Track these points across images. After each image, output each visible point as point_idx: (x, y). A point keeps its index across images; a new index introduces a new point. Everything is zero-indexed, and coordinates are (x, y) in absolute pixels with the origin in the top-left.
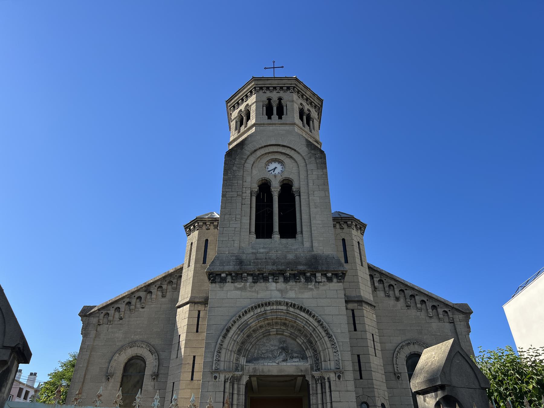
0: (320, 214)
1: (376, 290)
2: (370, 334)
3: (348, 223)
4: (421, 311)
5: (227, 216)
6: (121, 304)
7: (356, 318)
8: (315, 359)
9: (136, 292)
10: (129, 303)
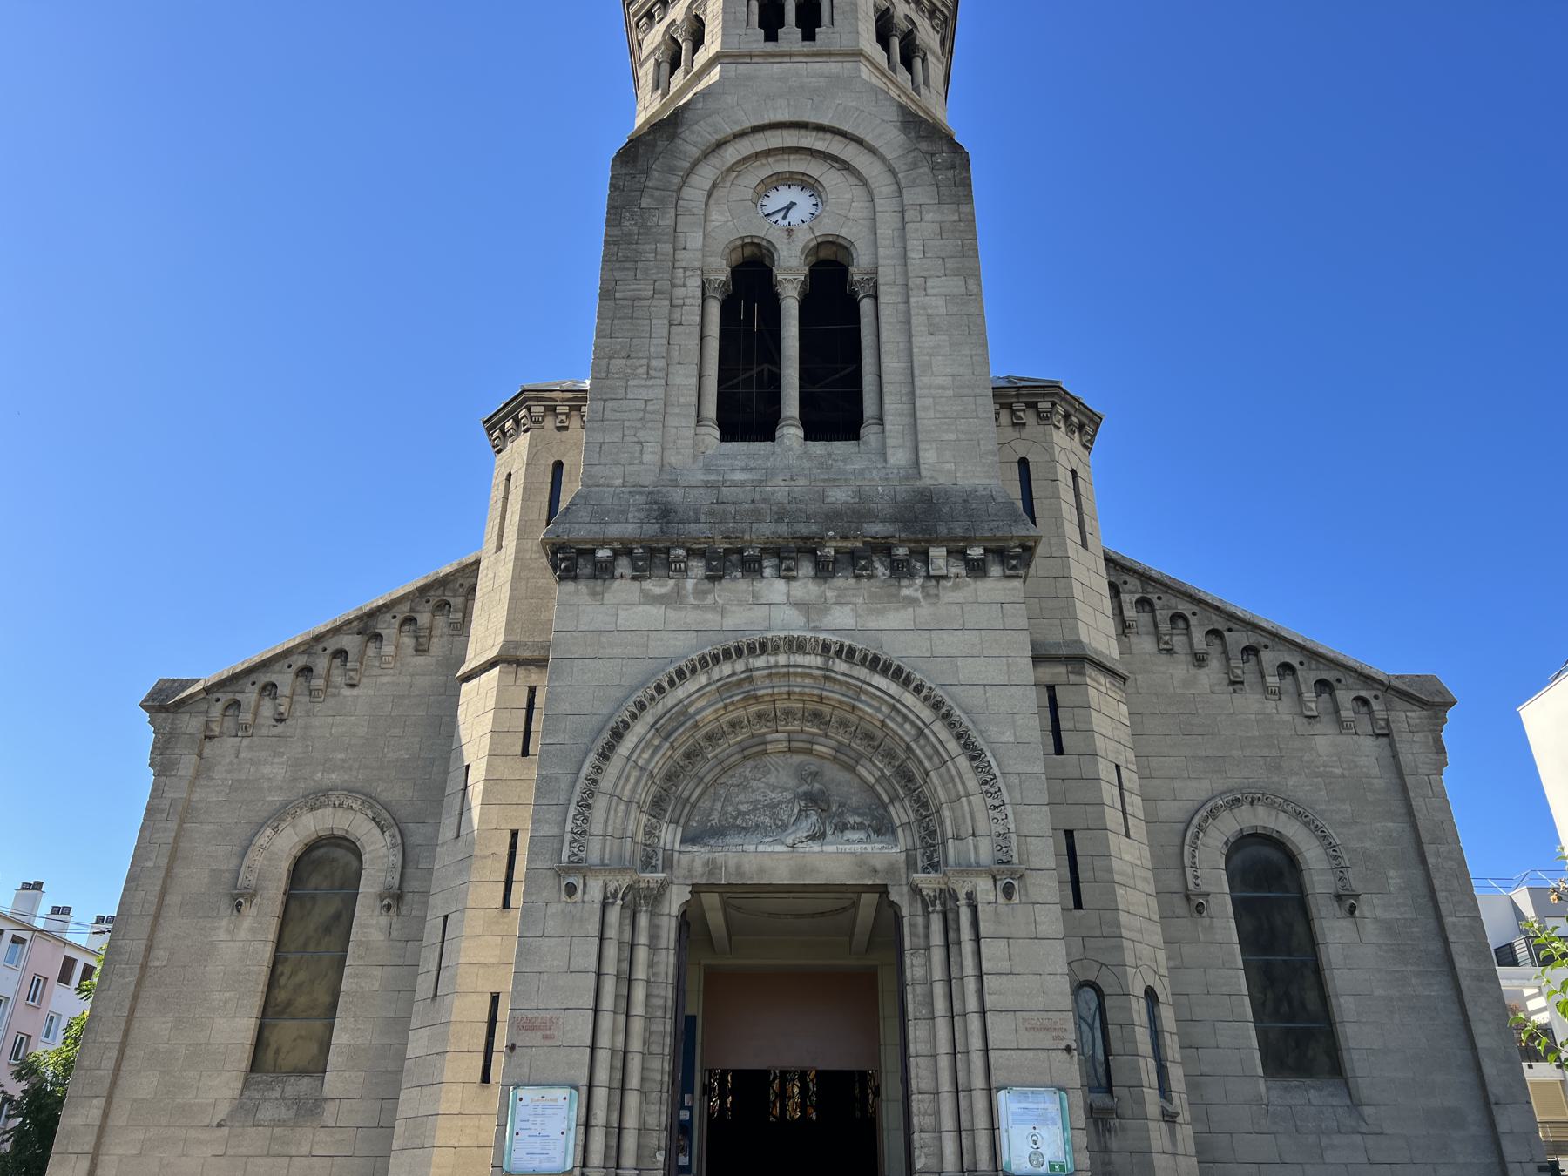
0: (946, 356)
1: (1127, 631)
2: (1109, 764)
3: (1040, 405)
4: (1280, 699)
5: (617, 363)
6: (281, 672)
7: (1062, 713)
8: (923, 834)
9: (327, 637)
10: (306, 671)
